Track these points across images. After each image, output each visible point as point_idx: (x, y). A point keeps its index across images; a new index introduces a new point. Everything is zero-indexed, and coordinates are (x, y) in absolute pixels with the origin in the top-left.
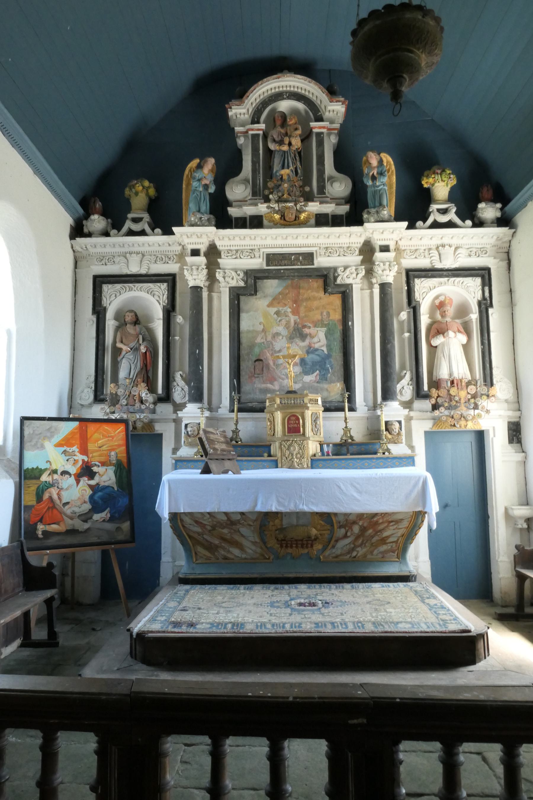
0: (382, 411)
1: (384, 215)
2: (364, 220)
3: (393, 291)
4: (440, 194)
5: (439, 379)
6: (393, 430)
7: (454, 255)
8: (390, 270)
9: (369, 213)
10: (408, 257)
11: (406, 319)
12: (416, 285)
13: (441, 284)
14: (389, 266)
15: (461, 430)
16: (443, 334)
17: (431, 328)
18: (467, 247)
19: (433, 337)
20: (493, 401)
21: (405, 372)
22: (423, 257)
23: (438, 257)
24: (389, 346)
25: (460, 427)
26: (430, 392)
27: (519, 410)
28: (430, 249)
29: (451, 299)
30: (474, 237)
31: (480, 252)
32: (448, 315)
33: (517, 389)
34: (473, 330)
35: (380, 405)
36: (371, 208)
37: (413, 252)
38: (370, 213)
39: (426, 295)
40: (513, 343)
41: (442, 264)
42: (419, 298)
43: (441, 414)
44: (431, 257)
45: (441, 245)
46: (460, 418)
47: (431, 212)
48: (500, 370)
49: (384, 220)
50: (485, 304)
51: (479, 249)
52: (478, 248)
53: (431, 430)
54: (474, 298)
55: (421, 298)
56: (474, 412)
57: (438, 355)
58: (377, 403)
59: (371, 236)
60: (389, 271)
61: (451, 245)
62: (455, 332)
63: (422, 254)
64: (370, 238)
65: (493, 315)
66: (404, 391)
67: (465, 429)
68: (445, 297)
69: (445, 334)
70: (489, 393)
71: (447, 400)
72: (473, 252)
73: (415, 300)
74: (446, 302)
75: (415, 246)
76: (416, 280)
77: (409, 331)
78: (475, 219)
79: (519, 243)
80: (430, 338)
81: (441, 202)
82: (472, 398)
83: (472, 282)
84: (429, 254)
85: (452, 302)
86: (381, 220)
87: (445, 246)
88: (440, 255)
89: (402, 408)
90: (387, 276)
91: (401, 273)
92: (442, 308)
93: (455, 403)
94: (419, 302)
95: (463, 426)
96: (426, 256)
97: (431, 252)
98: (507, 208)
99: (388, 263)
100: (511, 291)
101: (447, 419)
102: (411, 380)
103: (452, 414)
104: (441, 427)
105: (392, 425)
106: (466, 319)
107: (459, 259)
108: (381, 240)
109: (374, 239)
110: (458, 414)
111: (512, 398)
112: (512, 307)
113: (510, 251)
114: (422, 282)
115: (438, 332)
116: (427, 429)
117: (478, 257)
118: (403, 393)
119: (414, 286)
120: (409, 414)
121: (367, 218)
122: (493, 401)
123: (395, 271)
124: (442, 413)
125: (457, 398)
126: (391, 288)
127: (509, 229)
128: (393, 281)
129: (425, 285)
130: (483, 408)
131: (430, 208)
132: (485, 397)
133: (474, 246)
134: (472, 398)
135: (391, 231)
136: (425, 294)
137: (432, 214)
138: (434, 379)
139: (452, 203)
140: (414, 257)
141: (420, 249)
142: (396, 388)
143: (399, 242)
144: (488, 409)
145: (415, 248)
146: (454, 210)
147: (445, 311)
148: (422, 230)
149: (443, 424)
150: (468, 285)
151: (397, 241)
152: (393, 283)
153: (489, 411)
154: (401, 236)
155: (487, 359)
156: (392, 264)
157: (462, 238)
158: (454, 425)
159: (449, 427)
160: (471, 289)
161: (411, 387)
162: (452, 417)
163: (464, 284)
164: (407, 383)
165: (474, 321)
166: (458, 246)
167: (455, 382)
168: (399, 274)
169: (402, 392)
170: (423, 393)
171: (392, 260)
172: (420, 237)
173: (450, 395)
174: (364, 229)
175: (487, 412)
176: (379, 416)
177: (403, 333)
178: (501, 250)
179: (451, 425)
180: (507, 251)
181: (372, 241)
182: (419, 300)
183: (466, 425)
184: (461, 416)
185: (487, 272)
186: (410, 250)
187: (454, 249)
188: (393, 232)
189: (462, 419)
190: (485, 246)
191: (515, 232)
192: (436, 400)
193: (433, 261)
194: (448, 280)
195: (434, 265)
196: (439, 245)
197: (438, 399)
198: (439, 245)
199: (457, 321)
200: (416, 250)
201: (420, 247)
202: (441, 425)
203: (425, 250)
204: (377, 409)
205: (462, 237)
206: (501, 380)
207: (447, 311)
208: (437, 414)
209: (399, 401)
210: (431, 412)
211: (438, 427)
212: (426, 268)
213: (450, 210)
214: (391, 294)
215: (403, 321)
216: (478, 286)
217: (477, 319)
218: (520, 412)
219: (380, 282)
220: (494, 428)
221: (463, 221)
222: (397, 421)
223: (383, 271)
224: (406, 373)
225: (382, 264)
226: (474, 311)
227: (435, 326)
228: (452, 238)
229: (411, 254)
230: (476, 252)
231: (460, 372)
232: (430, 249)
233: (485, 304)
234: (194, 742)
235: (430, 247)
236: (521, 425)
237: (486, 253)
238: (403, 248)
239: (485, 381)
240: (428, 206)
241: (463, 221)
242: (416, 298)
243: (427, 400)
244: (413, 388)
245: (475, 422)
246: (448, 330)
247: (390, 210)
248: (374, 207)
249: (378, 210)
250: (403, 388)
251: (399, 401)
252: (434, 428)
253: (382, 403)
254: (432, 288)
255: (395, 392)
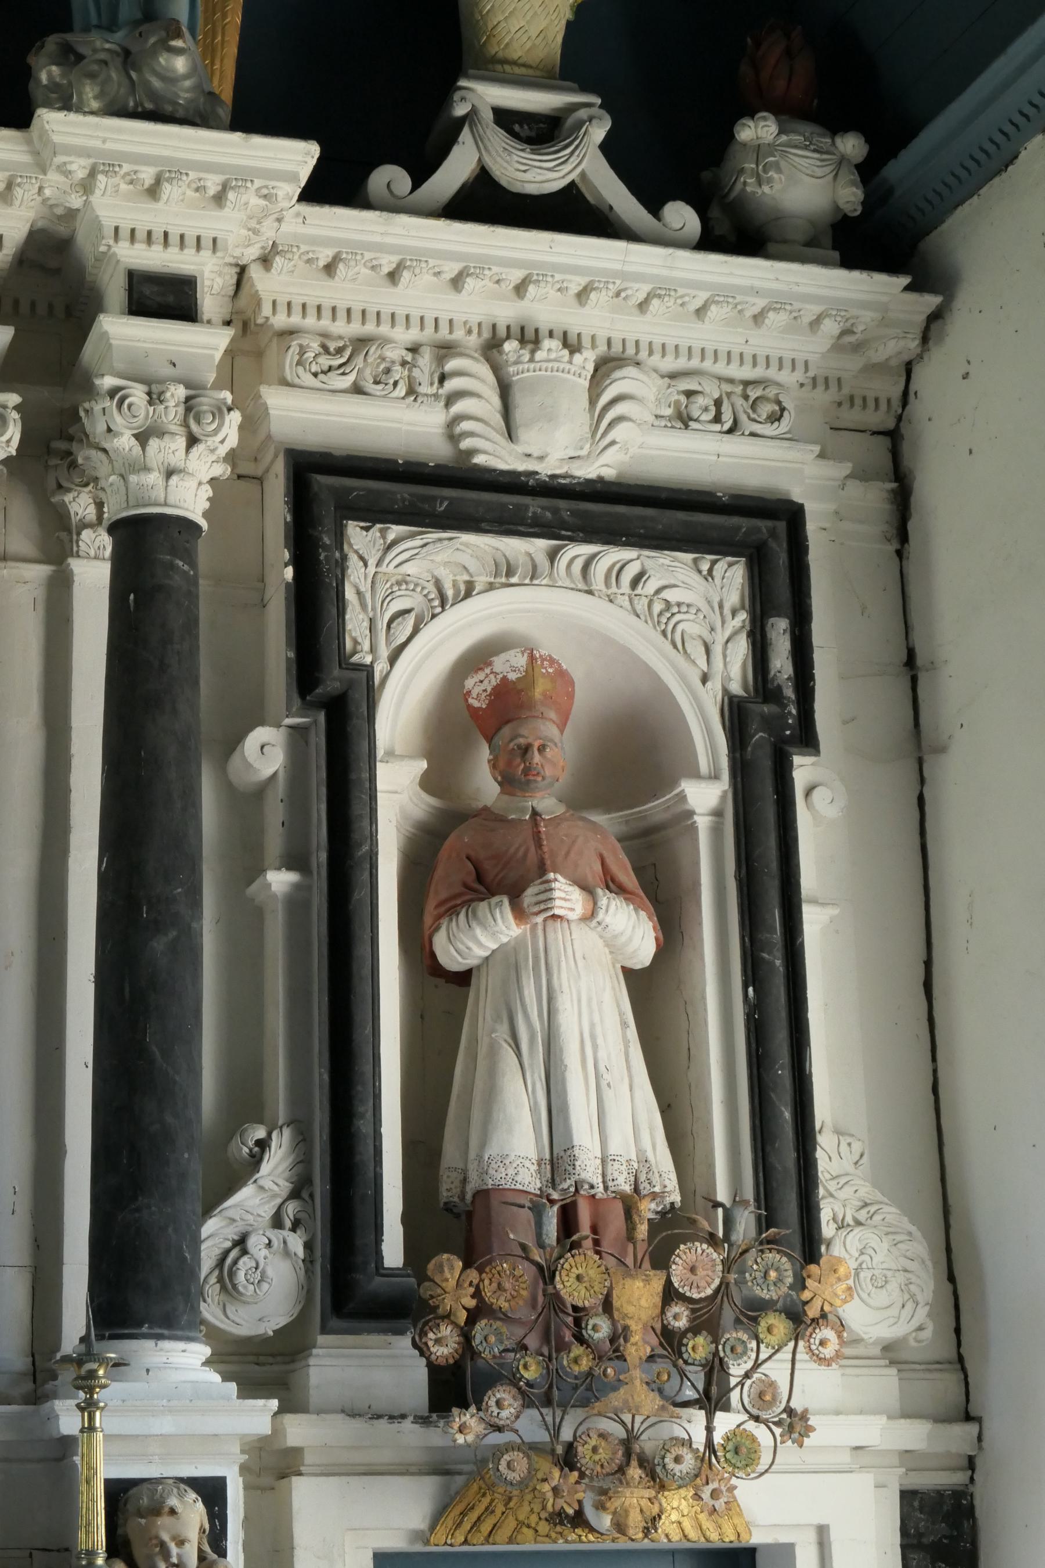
0: (88, 1407)
1: (171, 79)
2: (37, 94)
3: (204, 586)
4: (515, 25)
5: (483, 1195)
6: (166, 1554)
7: (593, 402)
8: (192, 441)
9: (70, 57)
10: (308, 380)
11: (281, 776)
12: (353, 561)
13: (510, 572)
14: (188, 410)
15: (623, 1544)
16: (515, 895)
17: (435, 851)
18: (669, 364)
19: (450, 909)
20: (828, 1352)
21: (261, 1133)
22: (401, 390)
23: (496, 401)
24: (159, 944)
25: (620, 1527)
26: (423, 1277)
27: (968, 1417)
28: (445, 350)
29: (562, 676)
30: (714, 310)
31: (739, 402)
32: (548, 772)
33: (951, 1278)
34: (697, 884)
35: (80, 1362)
36: (87, 29)
37: (339, 351)
38: (80, 58)
39: (416, 631)
40: (928, 986)
41: (520, 449)
42: (366, 646)
43: (496, 1438)
44: (451, 399)
45: (515, 331)
46: (621, 1470)
47: (461, 122)
48: (857, 1147)
49: (169, 108)
50: (772, 724)
51: (739, 389)
52: (731, 381)
53: (419, 1548)
54: (705, 679)
55: (384, 652)
56: (709, 1429)
57: (474, 1040)
58: (57, 1347)
59: (76, 201)
60: (181, 442)
61: (572, 339)
62: (587, 889)
63: (398, 373)
64: (71, 214)
65: (816, 794)
66: (245, 1263)
67: (646, 1544)
68: (532, 658)
69: (529, 896)
70: (806, 1295)
71: (533, 1341)
72: (700, 401)
73: (344, 661)
74: (538, 692)
75: (356, 316)
76: (354, 530)
77: (295, 861)
78: (715, 212)
79: (966, 376)
80: (428, 920)
81: (523, 71)
82: (694, 1329)
83: (695, 579)
84: (442, 379)
85: (571, 696)
86: (149, 106)
87: (536, 342)
88: (505, 390)
89: (232, 1387)
90: (170, 473)
91: (260, 480)
92: (506, 731)
93: (585, 1364)
94: (369, 670)
95: (635, 1521)
96: (424, 389)
97: (451, 365)
98: (894, 170)
99: (181, 392)
100: (910, 660)
101: (532, 1471)
102: (295, 1194)
103: (566, 1435)
104: (486, 1527)
105: (156, 1510)
106: (655, 809)
107: (618, 433)
108: (141, 235)
109: (97, 225)
110: (602, 1436)
111: (928, 1334)
112: (920, 762)
113: (905, 429)
114: (389, 547)
115: (480, 878)
116: (395, 1542)
117: (730, 431)
118: (241, 1276)
119: (342, 564)
120: (277, 1431)
121: (54, 87)
122: (828, 1352)
123: (223, 451)
124: (499, 1429)
125: (600, 1329)
126: (190, 558)
127: (908, 288)
128: (206, 515)
129: (410, 569)
130: (765, 1394)
131: (457, 96)
132: (778, 1325)
133: (708, 365)
134: (694, 1329)
135: (213, 183)
136: (410, 621)
137: (465, 134)
138: (447, 1189)
139: (584, 89)
140: (347, 381)
141: (384, 341)
142: (196, 1242)
143: (255, 273)
144: (796, 1404)
145: (356, 329)
146: (599, 132)
147: (526, 750)
148: (404, 219)
149: (500, 1508)
150: (670, 595)
151: (242, 271)
152: (204, 524)
153: (804, 1417)
154: (268, 232)
155: (782, 1072)
156: (205, 403)
157: (643, 306)
158: (579, 1520)
159: (544, 1527)
160: (691, 627)
161: (296, 1243)
162: (568, 1460)
163: (650, 587)
164: (267, 1211)
165: (703, 823)
166: (617, 348)
167: (584, 1216)
168: (243, 484)
169: (232, 1274)
170: (378, 1283)
171: (211, 377)
172: (388, 263)
173: (555, 1302)
174: (36, 153)
175: (791, 1428)
176: (67, 1444)
177: (256, 870)
178: (853, 416)
179: (558, 1518)
180: (891, 424)
181: (82, 239)
182: (368, 660)
183: (655, 1520)
184: (628, 1454)
185: (781, 526)
186: (325, 335)
187: (590, 367)
188: (219, 199)
189: (635, 1472)
190: (772, 373)
191: (936, 317)
192: (466, 1337)
193: (465, 426)
194: (553, 555)
195: (471, 452)
196: (502, 332)
197: (481, 1328)
198: (502, 332)
199: (600, 818)
200: (361, 343)
201: (385, 329)
202: (489, 1510)
203: (414, 350)
204: (54, 1395)
205: (641, 296)
206: (862, 1215)
207: (542, 749)
208: (470, 1438)
209: (213, 1335)
210: (423, 1421)
211: (467, 1525)
212: (422, 459)
213: (580, 124)
214: (192, 596)
215: (261, 790)
216: (727, 611)
217: (718, 813)
218: (973, 1429)
219: (114, 511)
220: (822, 1533)
221: (654, 207)
222: (194, 1483)
223: (142, 438)
224: (263, 1145)
225: (138, 394)
226: (704, 764)
227: (462, 839)
228: (582, 295)
229: (325, 361)
230: (718, 403)
231: (613, 1149)
232: (445, 350)
233: (772, 724)
234: (759, 432)
235: (444, 333)
236: (978, 1513)
237: (775, 418)
238: (280, 320)
239: (767, 1220)
240: (446, 89)
241: (654, 207)
242: (349, 645)
243: (401, 1332)
244: (308, 1246)
245: (715, 1494)
246: (542, 870)
247: (209, 51)
248: (111, 26)
249: (134, 48)
250: (241, 1242)
251: (213, 1335)
252: (440, 1535)
253: (97, 1347)
254: (450, 593)
255: (189, 1270)
